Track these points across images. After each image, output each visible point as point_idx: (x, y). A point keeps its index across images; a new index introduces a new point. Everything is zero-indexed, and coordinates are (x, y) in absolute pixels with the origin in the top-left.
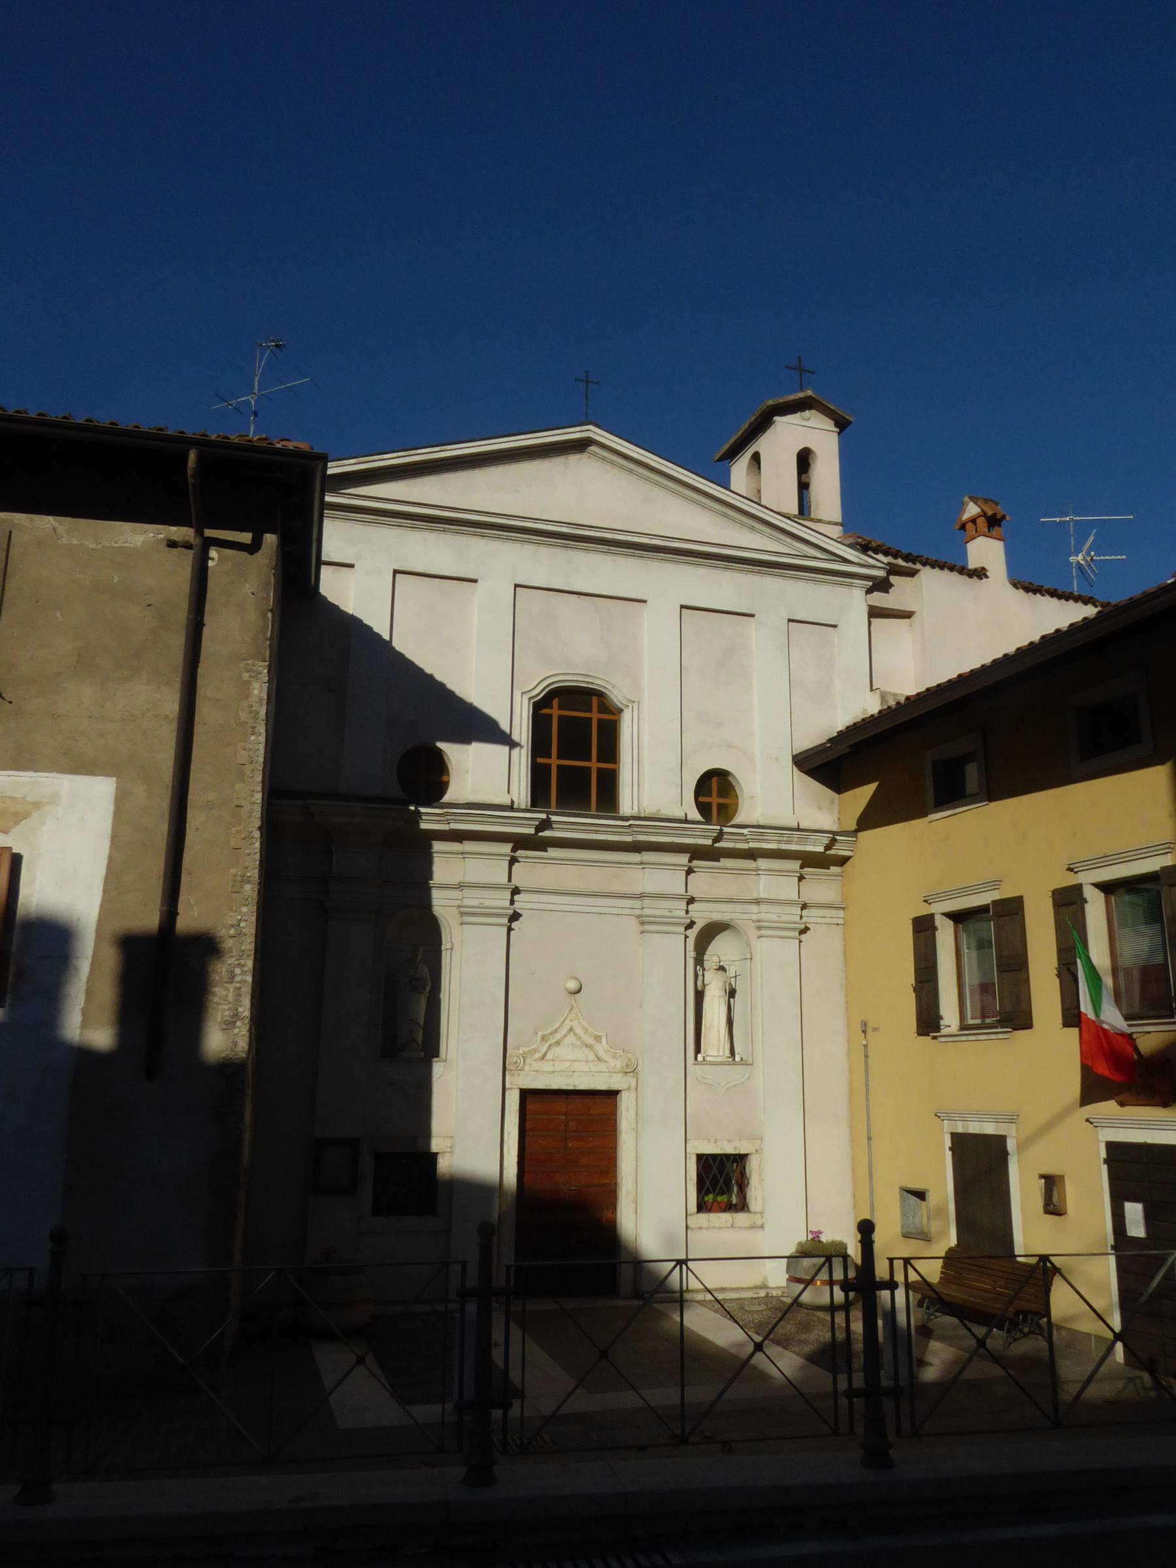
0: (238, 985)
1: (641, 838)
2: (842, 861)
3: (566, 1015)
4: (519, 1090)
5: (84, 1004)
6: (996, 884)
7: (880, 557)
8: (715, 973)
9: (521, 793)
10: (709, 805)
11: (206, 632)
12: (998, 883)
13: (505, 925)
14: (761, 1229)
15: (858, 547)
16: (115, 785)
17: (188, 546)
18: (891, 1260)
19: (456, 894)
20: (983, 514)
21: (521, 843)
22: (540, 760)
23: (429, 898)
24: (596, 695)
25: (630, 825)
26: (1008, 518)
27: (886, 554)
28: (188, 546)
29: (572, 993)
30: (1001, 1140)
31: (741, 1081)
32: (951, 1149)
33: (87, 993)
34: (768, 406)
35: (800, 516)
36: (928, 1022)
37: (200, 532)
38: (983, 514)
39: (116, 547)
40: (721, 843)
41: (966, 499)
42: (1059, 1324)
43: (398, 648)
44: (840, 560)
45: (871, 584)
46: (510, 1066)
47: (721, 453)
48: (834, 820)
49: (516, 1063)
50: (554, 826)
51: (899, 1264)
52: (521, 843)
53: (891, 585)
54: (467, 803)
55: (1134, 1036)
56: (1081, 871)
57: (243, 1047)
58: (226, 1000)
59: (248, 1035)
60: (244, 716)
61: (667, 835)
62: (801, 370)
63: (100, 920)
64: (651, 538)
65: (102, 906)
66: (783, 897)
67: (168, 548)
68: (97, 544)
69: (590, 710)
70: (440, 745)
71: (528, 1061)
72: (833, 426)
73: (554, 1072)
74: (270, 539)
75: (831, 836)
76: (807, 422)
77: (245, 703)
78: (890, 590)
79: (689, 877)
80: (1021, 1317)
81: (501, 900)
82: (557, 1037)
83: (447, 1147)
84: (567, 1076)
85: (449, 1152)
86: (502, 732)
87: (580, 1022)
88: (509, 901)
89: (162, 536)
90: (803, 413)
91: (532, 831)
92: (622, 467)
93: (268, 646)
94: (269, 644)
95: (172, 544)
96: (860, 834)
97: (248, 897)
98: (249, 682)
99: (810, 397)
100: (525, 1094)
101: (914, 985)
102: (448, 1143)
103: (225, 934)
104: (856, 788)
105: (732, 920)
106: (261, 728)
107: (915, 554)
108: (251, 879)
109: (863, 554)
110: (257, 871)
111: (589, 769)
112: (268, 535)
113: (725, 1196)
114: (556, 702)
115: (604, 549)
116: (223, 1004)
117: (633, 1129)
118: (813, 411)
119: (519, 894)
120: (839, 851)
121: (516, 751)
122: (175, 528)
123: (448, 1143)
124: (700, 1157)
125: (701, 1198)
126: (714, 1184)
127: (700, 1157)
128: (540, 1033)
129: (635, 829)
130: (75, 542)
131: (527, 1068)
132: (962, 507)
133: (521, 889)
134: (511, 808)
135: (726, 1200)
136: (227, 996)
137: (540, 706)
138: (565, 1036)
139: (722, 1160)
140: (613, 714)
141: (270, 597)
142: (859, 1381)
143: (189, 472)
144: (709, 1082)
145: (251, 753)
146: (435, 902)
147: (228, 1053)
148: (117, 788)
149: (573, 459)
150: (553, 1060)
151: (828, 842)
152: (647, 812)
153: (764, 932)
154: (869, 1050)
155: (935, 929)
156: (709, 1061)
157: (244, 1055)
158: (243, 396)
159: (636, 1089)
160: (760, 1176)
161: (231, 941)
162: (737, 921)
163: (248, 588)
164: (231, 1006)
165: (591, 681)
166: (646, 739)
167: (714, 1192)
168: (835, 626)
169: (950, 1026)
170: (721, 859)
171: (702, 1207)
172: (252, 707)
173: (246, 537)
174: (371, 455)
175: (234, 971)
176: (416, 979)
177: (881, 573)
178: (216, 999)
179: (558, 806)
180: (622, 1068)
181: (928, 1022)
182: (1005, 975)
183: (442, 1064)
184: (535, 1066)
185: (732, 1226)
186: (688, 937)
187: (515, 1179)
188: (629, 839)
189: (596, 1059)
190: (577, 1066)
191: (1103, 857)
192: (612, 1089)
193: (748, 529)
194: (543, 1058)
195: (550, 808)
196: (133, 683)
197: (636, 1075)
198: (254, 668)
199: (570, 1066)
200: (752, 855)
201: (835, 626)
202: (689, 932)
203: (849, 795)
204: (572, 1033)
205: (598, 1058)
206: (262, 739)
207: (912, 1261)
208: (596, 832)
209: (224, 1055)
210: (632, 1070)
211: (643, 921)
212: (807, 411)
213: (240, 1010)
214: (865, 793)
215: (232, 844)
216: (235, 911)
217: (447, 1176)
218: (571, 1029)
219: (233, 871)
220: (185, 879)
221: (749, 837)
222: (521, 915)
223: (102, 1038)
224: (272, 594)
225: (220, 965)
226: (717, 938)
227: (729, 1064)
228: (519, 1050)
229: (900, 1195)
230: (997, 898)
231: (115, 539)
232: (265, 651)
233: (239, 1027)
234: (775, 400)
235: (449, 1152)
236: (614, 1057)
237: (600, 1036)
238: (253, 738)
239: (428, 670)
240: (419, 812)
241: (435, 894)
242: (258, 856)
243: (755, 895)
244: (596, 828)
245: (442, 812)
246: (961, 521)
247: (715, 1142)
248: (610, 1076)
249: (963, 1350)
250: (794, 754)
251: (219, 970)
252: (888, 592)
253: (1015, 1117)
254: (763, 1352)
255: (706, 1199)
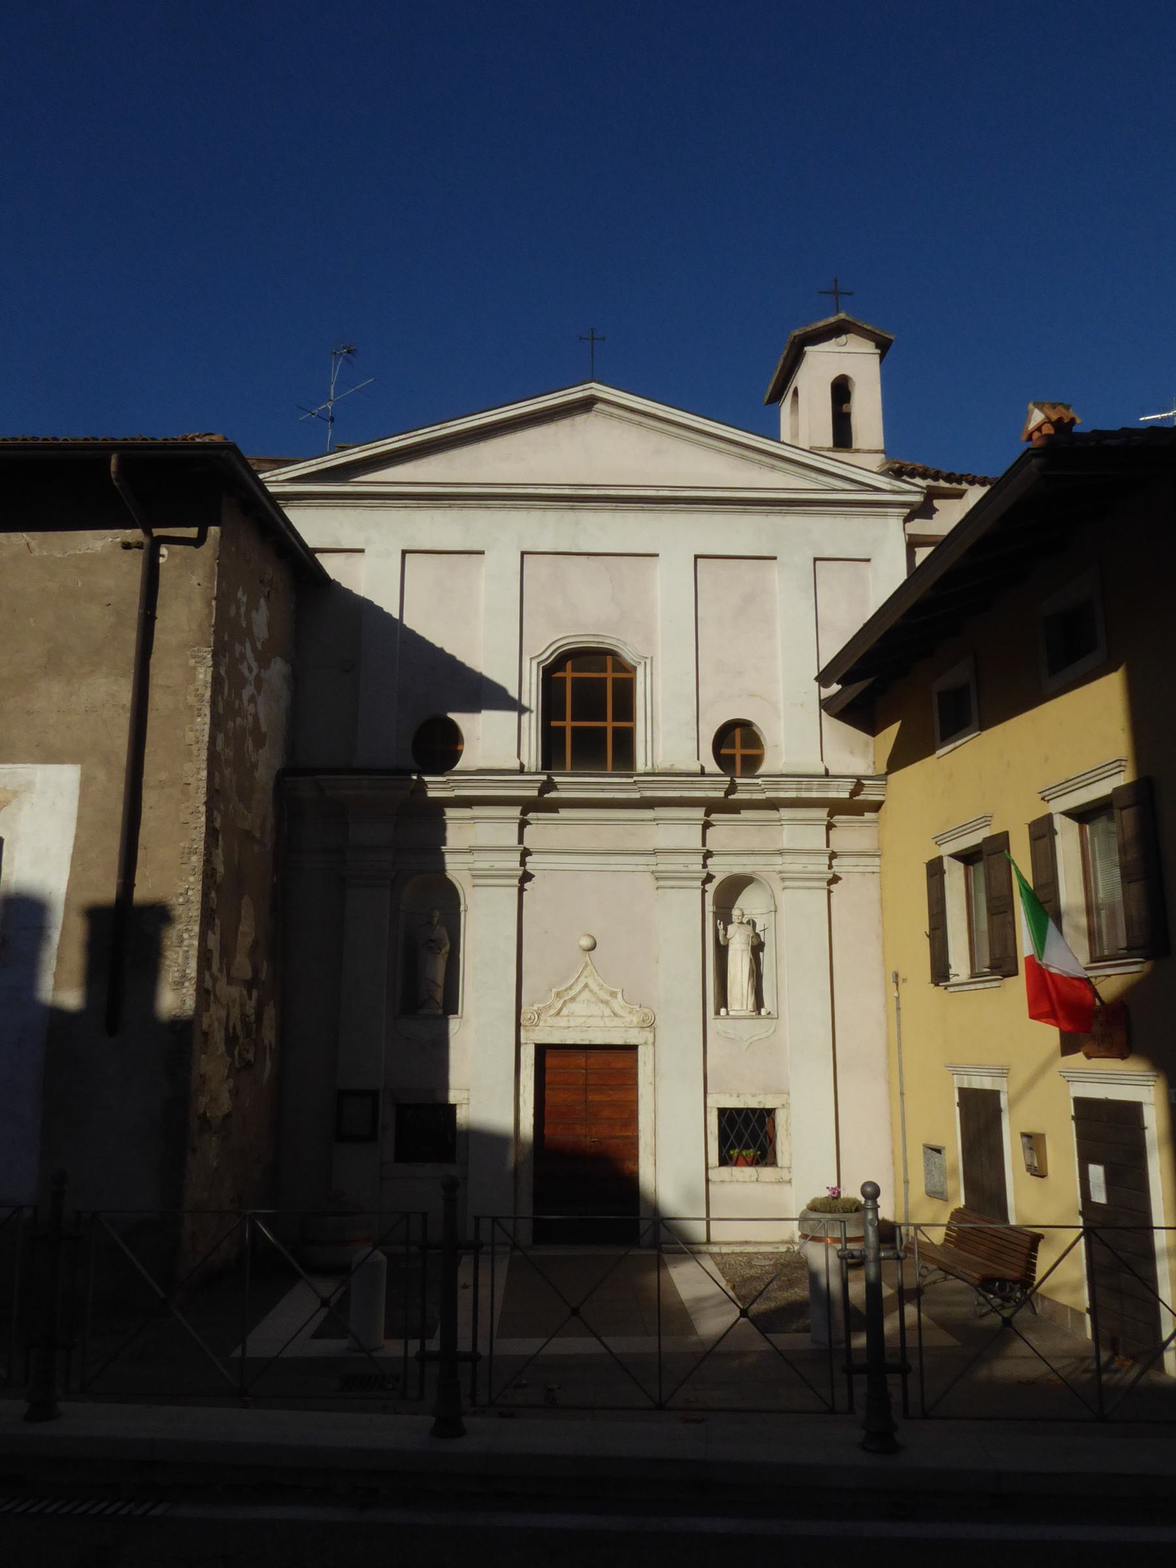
0: (186, 949)
1: (648, 794)
2: (877, 807)
3: (580, 972)
4: (534, 1045)
5: (56, 968)
6: (986, 820)
7: (918, 481)
8: (738, 927)
9: (532, 756)
10: (732, 757)
11: (158, 624)
12: (988, 819)
13: (698, 888)
14: (788, 1185)
16: (80, 772)
17: (139, 546)
18: (477, 1219)
20: (1046, 420)
21: (712, 807)
22: (554, 724)
23: (442, 863)
24: (610, 655)
25: (635, 781)
26: (1078, 421)
27: (924, 476)
28: (139, 546)
30: (995, 1095)
31: (767, 1035)
32: (959, 1105)
33: (57, 958)
34: (795, 337)
36: (940, 972)
37: (148, 532)
39: (79, 554)
40: (736, 794)
41: (1031, 406)
43: (408, 626)
44: (871, 489)
49: (530, 1019)
50: (558, 787)
52: (712, 807)
53: (935, 510)
54: (477, 770)
55: (1093, 980)
56: (1052, 799)
58: (175, 963)
60: (191, 699)
61: (675, 789)
62: (836, 293)
63: (68, 893)
64: (658, 490)
65: (70, 880)
66: (808, 846)
68: (64, 554)
70: (451, 715)
71: (542, 1017)
72: (874, 347)
73: (569, 1027)
75: (855, 780)
76: (843, 347)
77: (192, 688)
78: (934, 516)
79: (830, 832)
81: (512, 862)
82: (572, 993)
83: (464, 1099)
84: (582, 1031)
85: (466, 1104)
86: (512, 699)
87: (594, 979)
88: (827, 866)
89: (119, 540)
90: (838, 340)
91: (535, 793)
92: (629, 421)
93: (212, 633)
94: (214, 631)
95: (127, 546)
96: (891, 777)
97: (195, 867)
98: (195, 668)
99: (843, 320)
100: (542, 1051)
101: (928, 933)
102: (465, 1095)
103: (176, 902)
105: (753, 872)
106: (206, 710)
108: (198, 850)
109: (897, 480)
110: (202, 843)
111: (605, 729)
112: (212, 528)
114: (569, 665)
115: (612, 506)
117: (651, 1083)
118: (851, 336)
119: (531, 855)
120: (868, 795)
121: (525, 717)
122: (130, 531)
123: (465, 1095)
124: (722, 1112)
125: (724, 1151)
126: (739, 1142)
127: (722, 1112)
128: (554, 990)
130: (45, 554)
131: (541, 1024)
132: (1027, 415)
133: (531, 850)
134: (521, 771)
137: (550, 674)
138: (580, 992)
139: (747, 1114)
141: (214, 586)
142: (434, 1345)
144: (730, 1036)
145: (198, 734)
146: (448, 867)
147: (178, 1010)
149: (581, 420)
150: (568, 1016)
151: (852, 787)
152: (660, 768)
155: (944, 872)
156: (732, 1016)
157: (191, 1013)
159: (654, 1044)
160: (787, 1130)
162: (759, 873)
163: (195, 580)
164: (180, 968)
165: (601, 641)
166: (659, 698)
168: (868, 560)
169: (958, 975)
170: (742, 811)
171: (724, 1161)
173: (192, 532)
174: (372, 443)
175: (182, 936)
176: (432, 941)
177: (918, 498)
178: (168, 962)
179: (574, 765)
180: (638, 1023)
181: (940, 972)
182: (995, 917)
184: (550, 1021)
185: (757, 1181)
186: (832, 892)
187: (532, 1130)
188: (637, 795)
189: (612, 1014)
190: (591, 1022)
192: (628, 1043)
193: (768, 469)
194: (558, 1013)
195: (606, 771)
197: (652, 1029)
199: (585, 1022)
200: (773, 805)
201: (868, 560)
204: (587, 990)
205: (614, 1014)
206: (208, 720)
208: (603, 790)
209: (173, 1013)
210: (650, 1024)
211: (657, 879)
213: (188, 971)
215: (182, 819)
216: (185, 881)
217: (464, 1127)
218: (586, 986)
219: (182, 844)
221: (763, 786)
222: (533, 876)
223: (71, 998)
224: (216, 583)
225: (171, 931)
226: (744, 891)
227: (752, 1018)
228: (533, 1006)
229: (925, 1153)
230: (988, 835)
232: (210, 637)
233: (187, 987)
234: (802, 328)
235: (466, 1104)
236: (630, 1013)
237: (616, 992)
238: (199, 719)
239: (438, 645)
240: (424, 782)
241: (448, 858)
243: (780, 846)
244: (602, 787)
245: (445, 780)
247: (738, 1097)
248: (626, 1031)
249: (932, 1319)
250: (822, 698)
251: (171, 936)
252: (931, 518)
253: (1006, 1071)
254: (321, 1307)
255: (732, 1152)
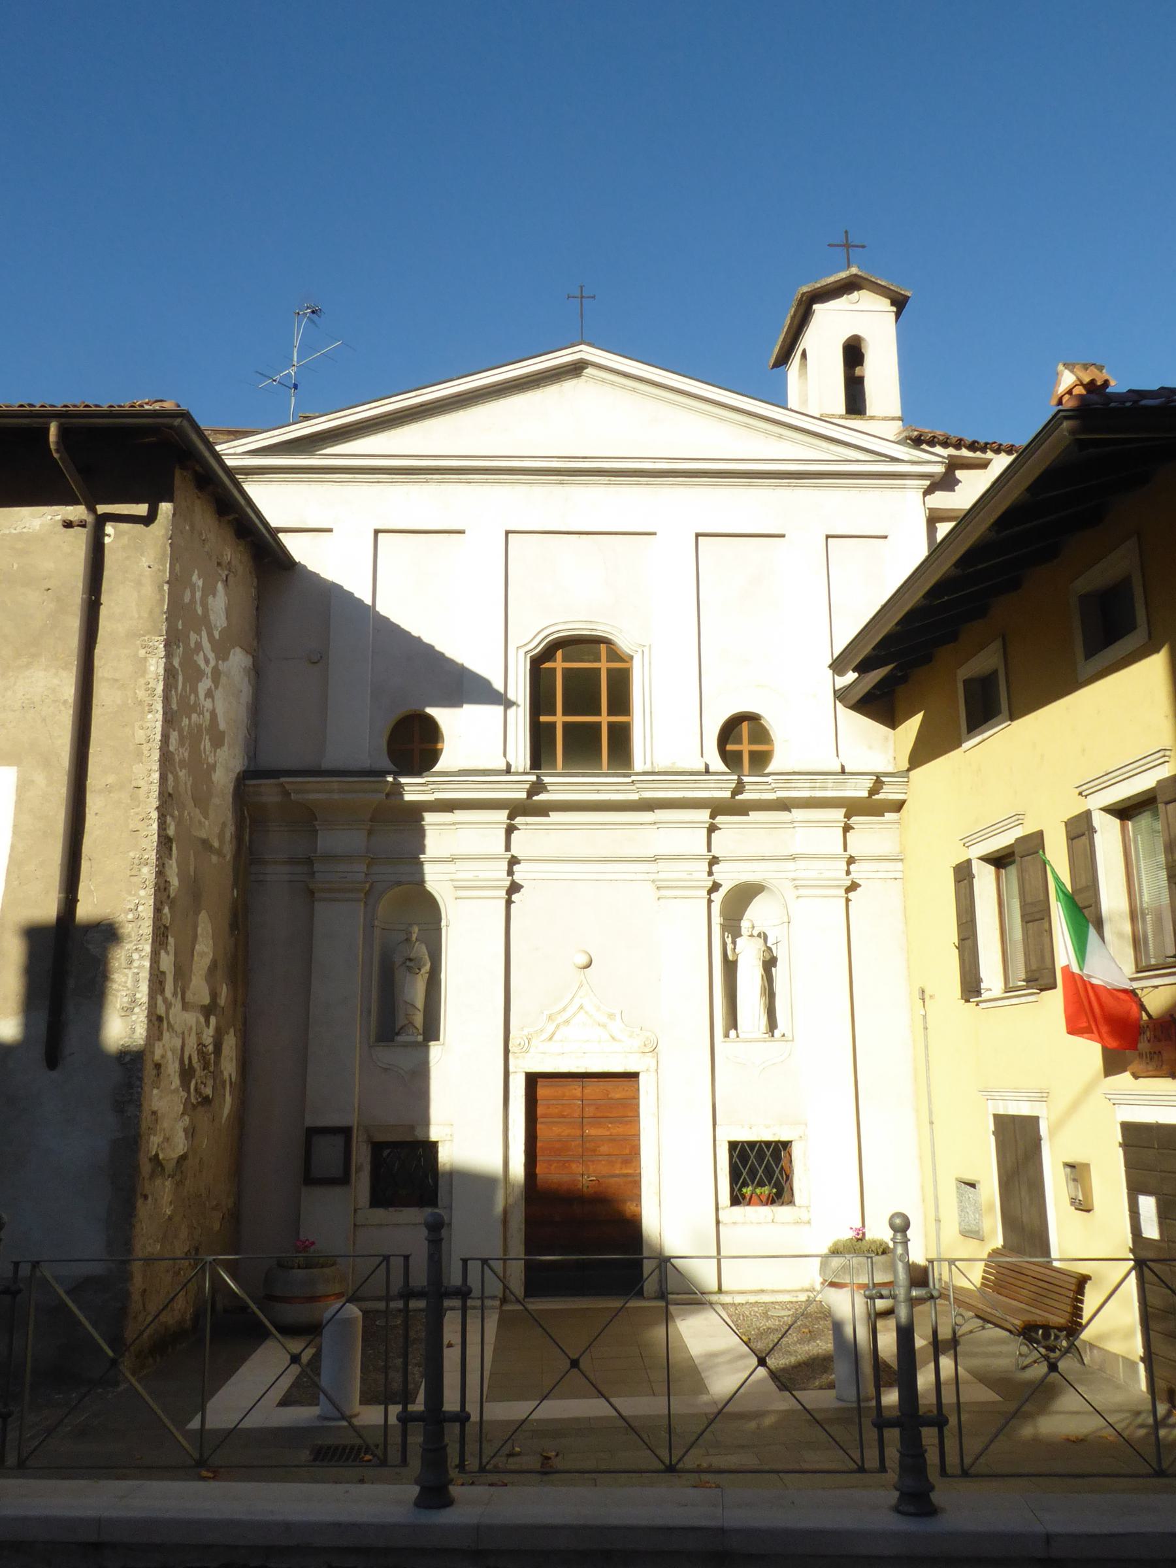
2: (898, 806)
4: (524, 1074)
6: (1018, 818)
7: (938, 449)
9: (520, 755)
10: (738, 755)
11: (104, 611)
12: (1021, 817)
15: (908, 441)
17: (83, 525)
19: (449, 867)
20: (1078, 383)
21: (718, 808)
22: (543, 719)
23: (421, 873)
24: (604, 643)
25: (633, 782)
27: (945, 444)
28: (83, 525)
29: (581, 968)
34: (803, 294)
35: (848, 416)
36: (971, 987)
37: (92, 509)
38: (1078, 383)
39: (15, 534)
41: (1061, 367)
42: (1091, 1342)
43: (382, 613)
45: (928, 483)
46: (514, 1048)
47: (774, 357)
48: (889, 760)
49: (520, 1044)
50: (549, 788)
51: (474, 1268)
52: (718, 808)
53: (958, 482)
57: (140, 1034)
59: (146, 1022)
60: (141, 694)
62: (847, 246)
67: (65, 529)
69: (598, 660)
74: (165, 508)
77: (142, 681)
78: (956, 488)
80: (1040, 1332)
82: (565, 1016)
86: (497, 692)
89: (59, 517)
90: (849, 296)
91: (523, 795)
92: (623, 387)
94: (166, 617)
95: (68, 525)
96: (912, 773)
98: (145, 659)
100: (532, 1080)
101: (957, 945)
104: (906, 721)
105: (764, 879)
107: (982, 441)
112: (163, 504)
113: (766, 1187)
114: (559, 653)
116: (123, 990)
118: (863, 293)
120: (889, 793)
121: (512, 712)
124: (733, 1145)
127: (733, 1145)
129: (638, 786)
132: (1056, 378)
134: (508, 771)
135: (767, 1192)
136: (126, 982)
137: (538, 664)
138: (575, 1014)
140: (627, 662)
143: (53, 447)
146: (428, 877)
147: (127, 1039)
148: (18, 777)
151: (871, 785)
153: (802, 892)
154: (928, 1021)
157: (142, 1042)
158: (285, 371)
161: (130, 926)
162: (769, 880)
163: (145, 562)
167: (753, 1183)
168: (886, 537)
169: (991, 990)
172: (149, 683)
173: (142, 509)
176: (410, 960)
178: (115, 986)
181: (971, 987)
183: (440, 1047)
188: (634, 797)
191: (1105, 775)
195: (556, 770)
196: (33, 670)
198: (151, 644)
200: (784, 805)
202: (714, 896)
203: (902, 728)
205: (613, 1038)
207: (490, 1262)
208: (598, 791)
209: (122, 1043)
210: (652, 1049)
212: (856, 293)
213: (138, 996)
214: (913, 725)
215: (132, 826)
216: (134, 895)
218: (581, 1007)
219: (132, 854)
220: (85, 866)
221: (774, 785)
224: (168, 565)
225: (119, 951)
226: (754, 900)
229: (958, 1188)
231: (13, 526)
238: (150, 716)
239: (415, 633)
240: (400, 785)
241: (428, 868)
242: (156, 836)
246: (1058, 395)
252: (953, 490)
253: (1045, 1095)
